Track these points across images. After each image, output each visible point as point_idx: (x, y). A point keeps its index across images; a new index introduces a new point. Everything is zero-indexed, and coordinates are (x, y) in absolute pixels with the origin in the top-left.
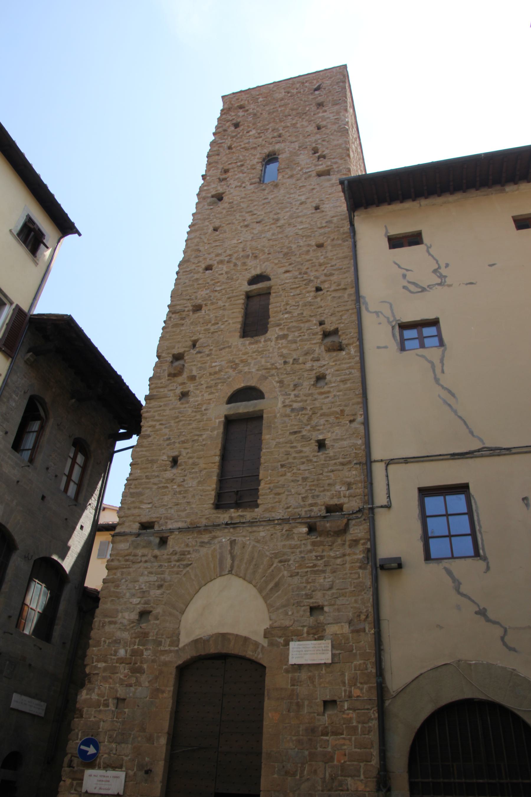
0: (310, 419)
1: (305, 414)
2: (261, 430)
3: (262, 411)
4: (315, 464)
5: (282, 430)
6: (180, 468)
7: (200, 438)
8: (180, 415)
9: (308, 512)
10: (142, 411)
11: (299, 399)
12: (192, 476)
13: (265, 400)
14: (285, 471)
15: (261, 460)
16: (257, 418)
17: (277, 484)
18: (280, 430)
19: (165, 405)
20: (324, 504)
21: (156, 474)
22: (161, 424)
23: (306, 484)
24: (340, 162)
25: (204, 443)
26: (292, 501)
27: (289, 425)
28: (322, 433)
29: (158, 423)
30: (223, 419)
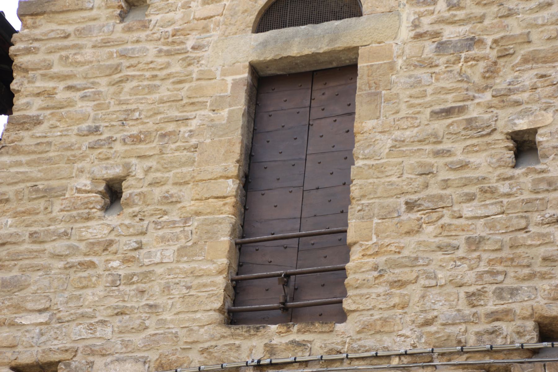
0: (492, 72)
1: (476, 59)
2: (351, 104)
3: (355, 50)
4: (505, 200)
5: (411, 106)
6: (128, 211)
7: (183, 129)
8: (125, 63)
9: (486, 337)
10: (12, 48)
11: (461, 14)
12: (161, 233)
13: (362, 19)
14: (419, 220)
15: (352, 188)
16: (340, 70)
17: (397, 256)
18: (403, 106)
19: (80, 33)
20: (532, 315)
21: (61, 228)
22: (69, 88)
23: (479, 258)
25: (194, 141)
26: (441, 306)
27: (430, 90)
28: (523, 114)
29: (61, 85)
30: (245, 75)
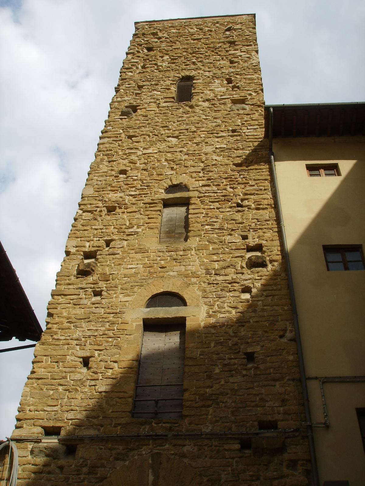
24: (254, 94)
30: (141, 323)
